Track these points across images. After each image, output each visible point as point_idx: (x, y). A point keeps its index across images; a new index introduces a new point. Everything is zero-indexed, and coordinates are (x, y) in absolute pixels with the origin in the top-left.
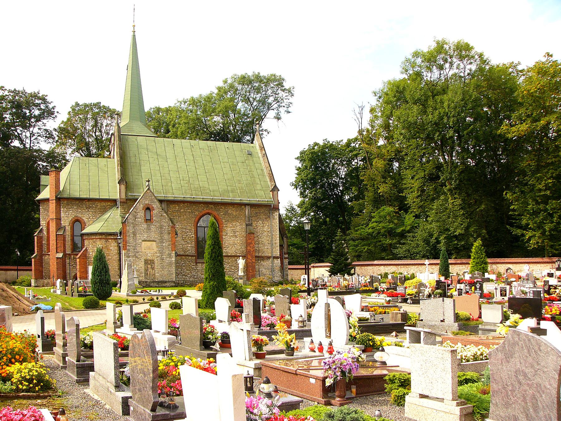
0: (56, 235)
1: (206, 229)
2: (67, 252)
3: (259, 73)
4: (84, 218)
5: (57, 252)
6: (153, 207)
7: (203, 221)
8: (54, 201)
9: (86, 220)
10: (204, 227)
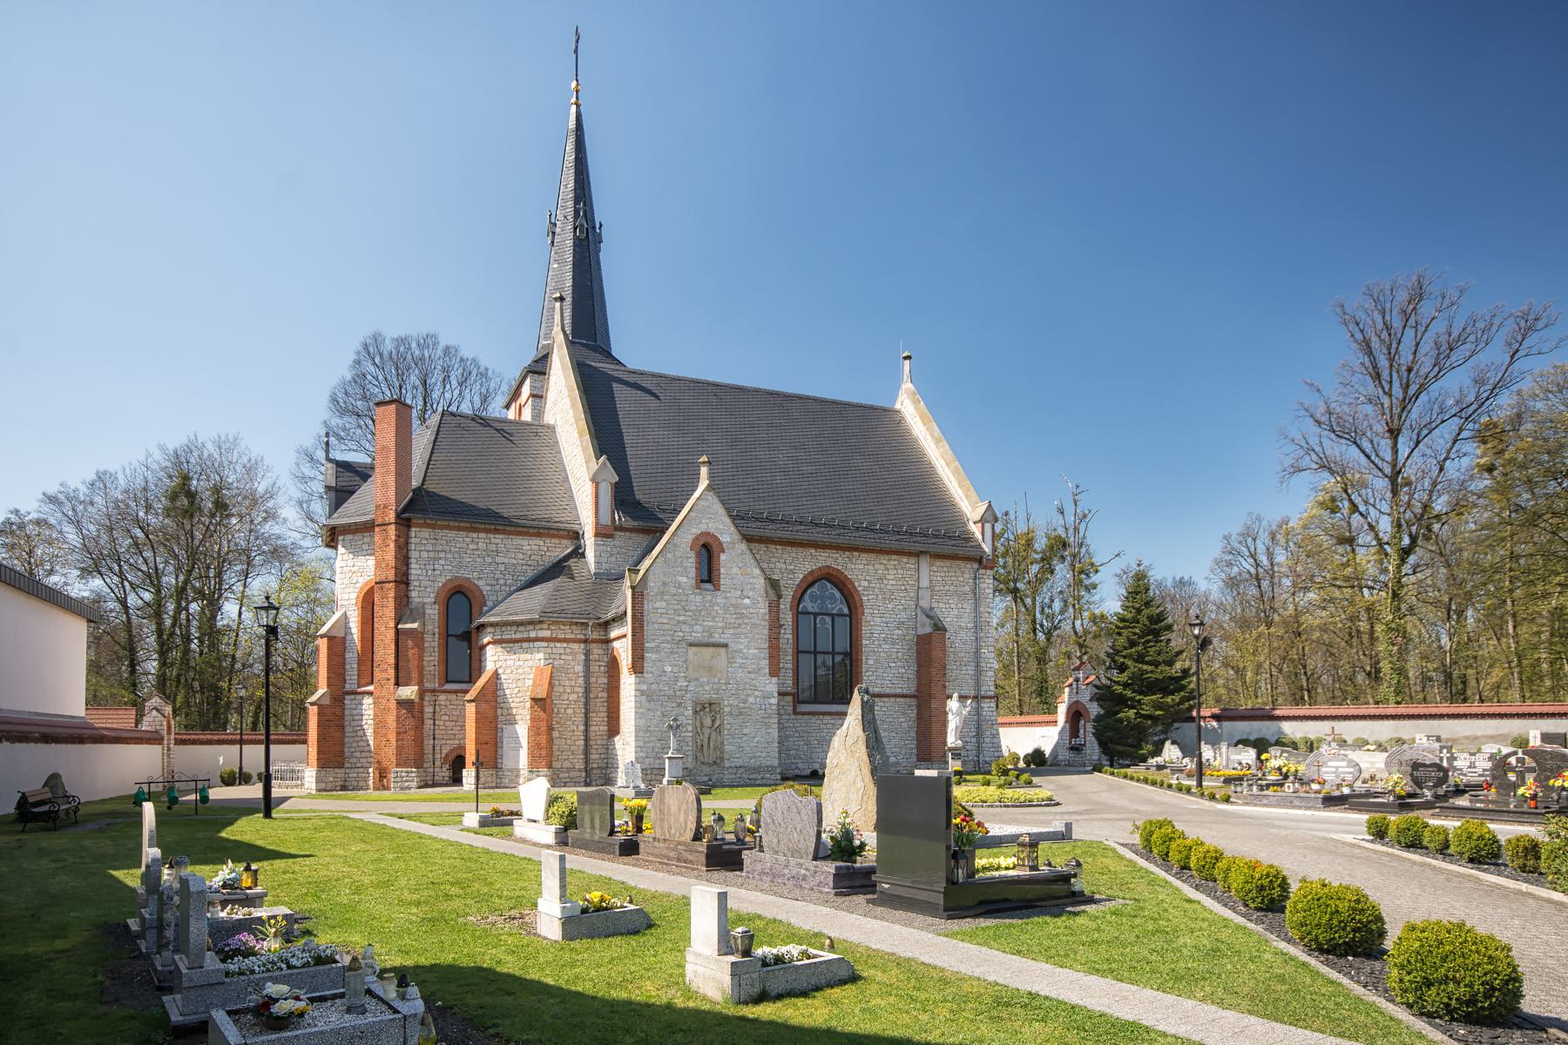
0: (397, 632)
1: (819, 618)
2: (427, 685)
3: (1149, 567)
4: (480, 583)
5: (397, 684)
6: (721, 544)
7: (813, 599)
8: (393, 527)
9: (486, 589)
10: (815, 615)
